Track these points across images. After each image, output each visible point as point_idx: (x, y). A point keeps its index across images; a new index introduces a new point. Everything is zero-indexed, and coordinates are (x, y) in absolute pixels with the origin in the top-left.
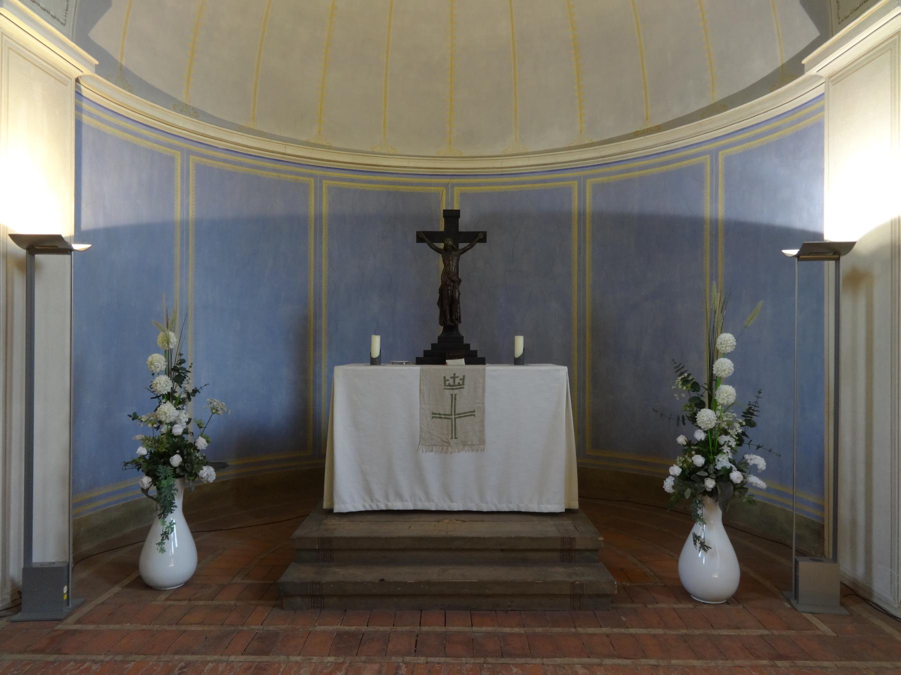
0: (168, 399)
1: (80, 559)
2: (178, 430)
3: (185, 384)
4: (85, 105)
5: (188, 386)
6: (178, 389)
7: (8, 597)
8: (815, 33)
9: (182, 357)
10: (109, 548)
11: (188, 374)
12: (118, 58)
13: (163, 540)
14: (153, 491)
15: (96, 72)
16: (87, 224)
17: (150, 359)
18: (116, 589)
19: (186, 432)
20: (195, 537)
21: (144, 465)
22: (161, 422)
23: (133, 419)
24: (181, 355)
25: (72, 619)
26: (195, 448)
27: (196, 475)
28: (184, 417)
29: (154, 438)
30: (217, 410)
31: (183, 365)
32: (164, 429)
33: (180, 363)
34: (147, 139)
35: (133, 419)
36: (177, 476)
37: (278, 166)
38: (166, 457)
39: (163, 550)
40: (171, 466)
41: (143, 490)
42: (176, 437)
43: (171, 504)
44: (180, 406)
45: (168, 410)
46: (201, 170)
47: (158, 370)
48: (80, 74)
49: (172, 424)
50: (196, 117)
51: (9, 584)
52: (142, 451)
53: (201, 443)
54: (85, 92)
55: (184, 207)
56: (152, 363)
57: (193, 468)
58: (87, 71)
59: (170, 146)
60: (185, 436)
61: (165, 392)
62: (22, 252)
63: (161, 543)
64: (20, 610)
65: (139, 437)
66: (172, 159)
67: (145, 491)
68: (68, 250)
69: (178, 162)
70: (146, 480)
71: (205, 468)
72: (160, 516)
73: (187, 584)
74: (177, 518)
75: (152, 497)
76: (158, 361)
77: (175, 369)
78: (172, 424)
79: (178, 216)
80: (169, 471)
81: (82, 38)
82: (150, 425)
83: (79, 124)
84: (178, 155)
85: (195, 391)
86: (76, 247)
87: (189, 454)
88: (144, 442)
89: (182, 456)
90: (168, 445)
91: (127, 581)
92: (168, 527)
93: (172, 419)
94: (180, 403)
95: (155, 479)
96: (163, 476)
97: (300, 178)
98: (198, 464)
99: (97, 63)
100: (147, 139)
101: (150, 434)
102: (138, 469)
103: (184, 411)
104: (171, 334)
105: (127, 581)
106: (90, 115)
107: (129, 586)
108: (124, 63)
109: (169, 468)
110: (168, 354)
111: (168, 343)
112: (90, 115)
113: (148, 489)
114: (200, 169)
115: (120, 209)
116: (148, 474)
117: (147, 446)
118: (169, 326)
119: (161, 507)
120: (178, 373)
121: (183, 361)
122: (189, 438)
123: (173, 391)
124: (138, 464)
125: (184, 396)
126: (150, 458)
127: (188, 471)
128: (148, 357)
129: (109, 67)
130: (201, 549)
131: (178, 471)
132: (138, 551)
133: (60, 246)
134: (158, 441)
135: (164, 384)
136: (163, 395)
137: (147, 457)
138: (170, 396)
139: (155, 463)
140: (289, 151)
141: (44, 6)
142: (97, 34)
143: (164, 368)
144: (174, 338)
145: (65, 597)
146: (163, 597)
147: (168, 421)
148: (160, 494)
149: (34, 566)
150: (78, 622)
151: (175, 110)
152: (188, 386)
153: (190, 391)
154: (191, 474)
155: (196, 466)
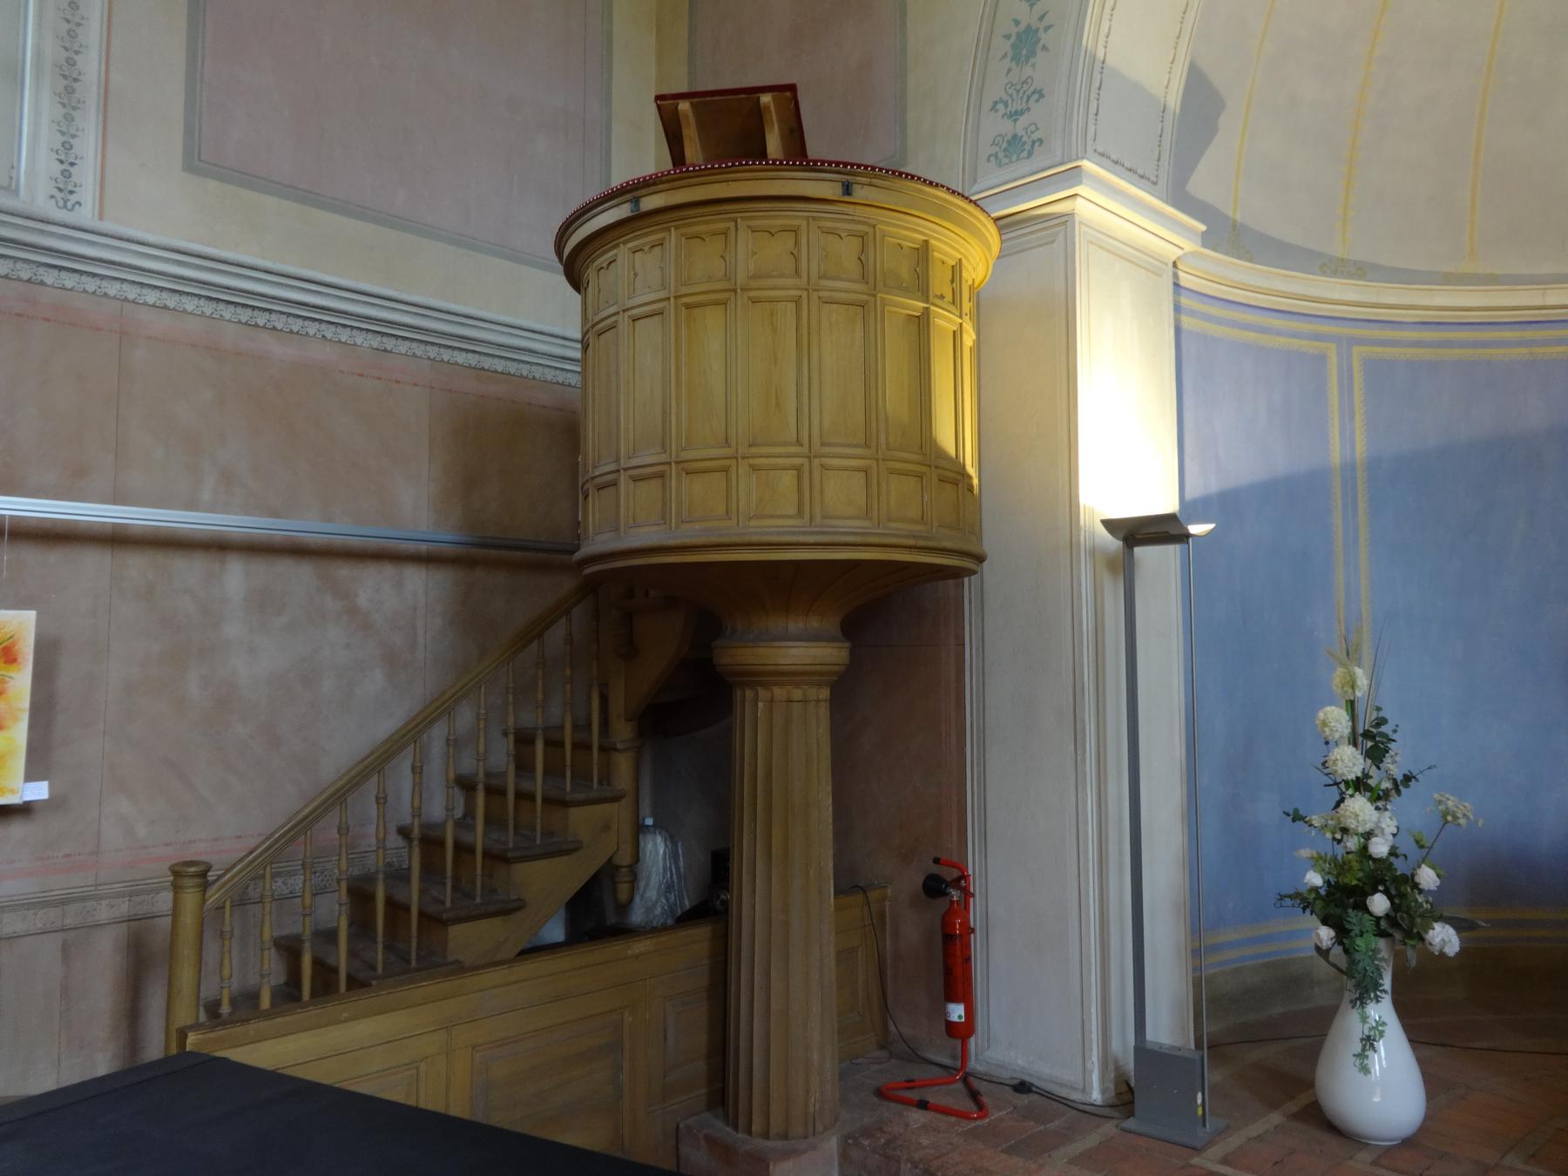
0: (1357, 789)
1: (1216, 1047)
2: (1379, 848)
3: (1387, 763)
4: (1185, 301)
5: (1395, 765)
6: (1373, 771)
7: (1112, 1086)
8: (1150, 1035)
9: (1382, 714)
10: (1262, 1041)
11: (1392, 745)
12: (1230, 213)
13: (1364, 1050)
14: (1342, 961)
15: (1204, 245)
16: (1195, 490)
17: (1321, 715)
18: (1276, 1118)
19: (1393, 852)
20: (1414, 1049)
21: (1319, 904)
22: (1345, 830)
23: (1294, 820)
24: (1379, 709)
25: (1216, 1151)
26: (1416, 886)
27: (1422, 939)
28: (1389, 824)
29: (1335, 858)
30: (1455, 818)
31: (1383, 729)
32: (1352, 843)
33: (1378, 725)
34: (1279, 333)
35: (1294, 820)
36: (1382, 934)
37: (1530, 334)
38: (1350, 889)
39: (1365, 1070)
40: (1371, 914)
41: (1318, 949)
42: (1375, 860)
43: (1376, 986)
44: (1380, 804)
45: (1359, 809)
46: (1374, 368)
47: (1337, 736)
48: (1179, 253)
49: (1368, 835)
50: (1361, 277)
51: (1111, 1066)
52: (1315, 879)
53: (1428, 877)
54: (1186, 280)
55: (1346, 439)
56: (1325, 724)
57: (1412, 923)
58: (1189, 246)
59: (1317, 337)
60: (1392, 859)
61: (1351, 777)
62: (1113, 543)
63: (1362, 1056)
64: (1131, 1114)
65: (1305, 853)
66: (1322, 359)
67: (1323, 953)
68: (1184, 537)
69: (1333, 361)
70: (1326, 934)
71: (1438, 927)
72: (1353, 1003)
73: (1408, 1143)
74: (1382, 1011)
75: (1334, 966)
76: (1336, 719)
77: (1367, 735)
78: (1368, 835)
79: (1336, 455)
80: (1369, 924)
81: (1181, 198)
82: (1329, 835)
83: (1178, 330)
84: (1331, 350)
85: (1408, 779)
86: (1195, 529)
87: (1403, 896)
88: (1317, 862)
89: (1390, 898)
90: (1360, 875)
91: (1293, 1107)
92: (1372, 1028)
93: (1368, 827)
94: (1379, 798)
95: (1342, 933)
96: (1356, 930)
97: (1537, 350)
98: (1422, 916)
99: (1203, 228)
100: (1279, 333)
101: (1327, 848)
102: (1304, 910)
103: (1388, 814)
104: (1359, 672)
105: (1293, 1107)
106: (1192, 313)
107: (1296, 1116)
108: (1238, 218)
109: (1367, 916)
110: (1351, 706)
111: (1353, 687)
112: (1192, 313)
113: (1328, 950)
114: (1371, 366)
115: (1244, 463)
116: (1325, 922)
117: (1322, 871)
118: (1351, 654)
119: (1357, 986)
120: (1374, 744)
121: (1381, 722)
122: (1400, 867)
123: (1366, 776)
124: (1306, 901)
125: (1386, 785)
126: (1328, 894)
127: (1405, 924)
128: (1317, 711)
129: (1226, 234)
130: (1433, 1083)
131: (1383, 924)
132: (1313, 1054)
133: (1173, 532)
134: (1341, 867)
135: (1350, 762)
136: (1347, 783)
137: (1323, 892)
138: (1360, 784)
139: (1339, 902)
140: (1552, 300)
141: (1114, 157)
142: (1200, 184)
143: (1347, 731)
144: (1362, 679)
145: (1200, 1112)
146: (1365, 1157)
147: (1360, 830)
148: (1353, 962)
149: (1149, 1046)
150: (1225, 1161)
151: (1324, 273)
152: (1395, 765)
153: (1400, 778)
154: (1408, 934)
155: (1418, 920)
